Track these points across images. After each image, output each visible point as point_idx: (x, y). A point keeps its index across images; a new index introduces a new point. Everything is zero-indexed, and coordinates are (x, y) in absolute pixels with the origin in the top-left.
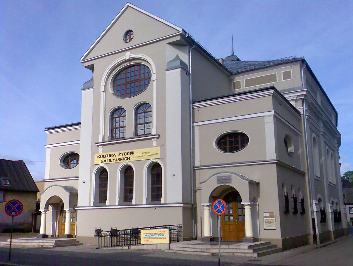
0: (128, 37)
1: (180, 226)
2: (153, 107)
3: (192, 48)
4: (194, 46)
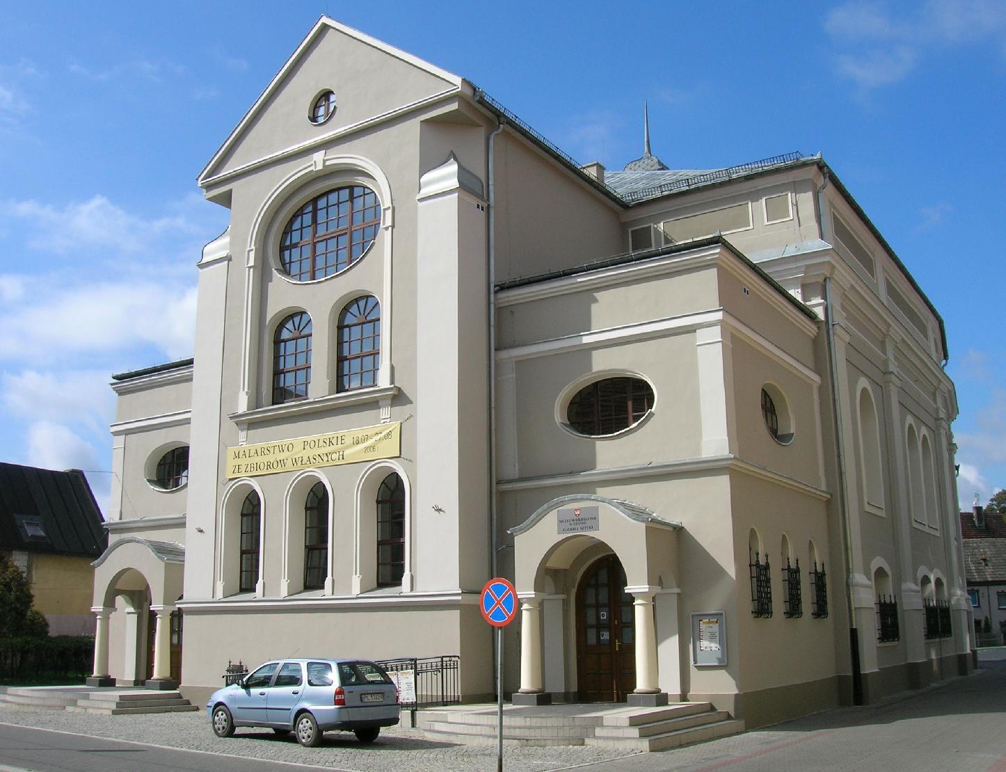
0: (322, 111)
1: (453, 659)
2: (382, 306)
3: (496, 132)
4: (502, 126)
